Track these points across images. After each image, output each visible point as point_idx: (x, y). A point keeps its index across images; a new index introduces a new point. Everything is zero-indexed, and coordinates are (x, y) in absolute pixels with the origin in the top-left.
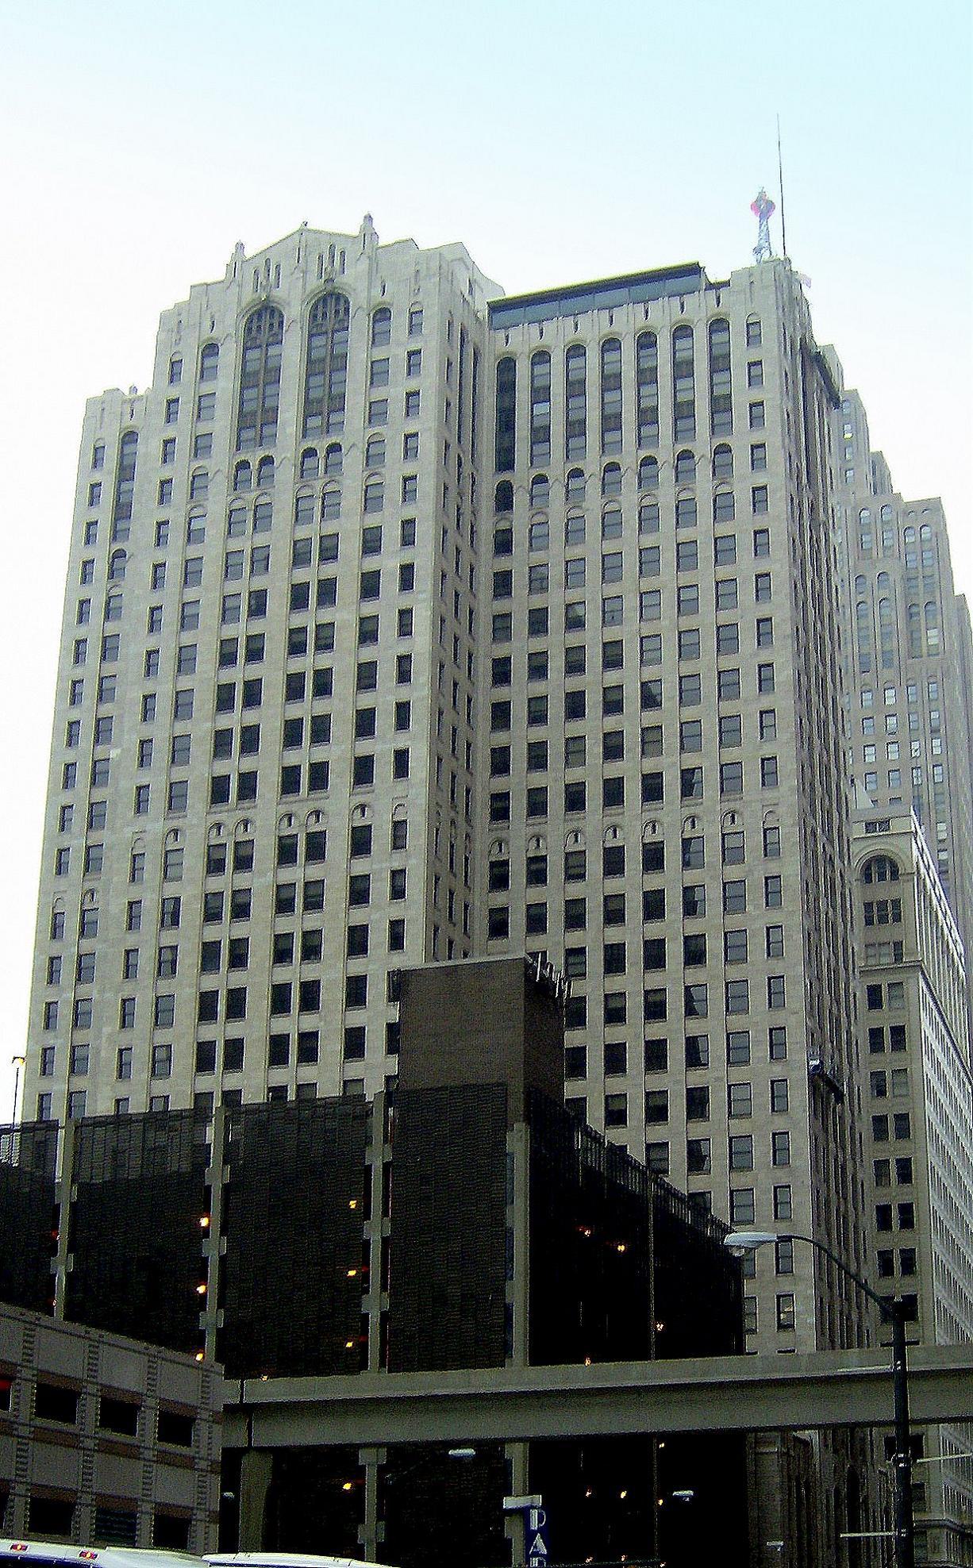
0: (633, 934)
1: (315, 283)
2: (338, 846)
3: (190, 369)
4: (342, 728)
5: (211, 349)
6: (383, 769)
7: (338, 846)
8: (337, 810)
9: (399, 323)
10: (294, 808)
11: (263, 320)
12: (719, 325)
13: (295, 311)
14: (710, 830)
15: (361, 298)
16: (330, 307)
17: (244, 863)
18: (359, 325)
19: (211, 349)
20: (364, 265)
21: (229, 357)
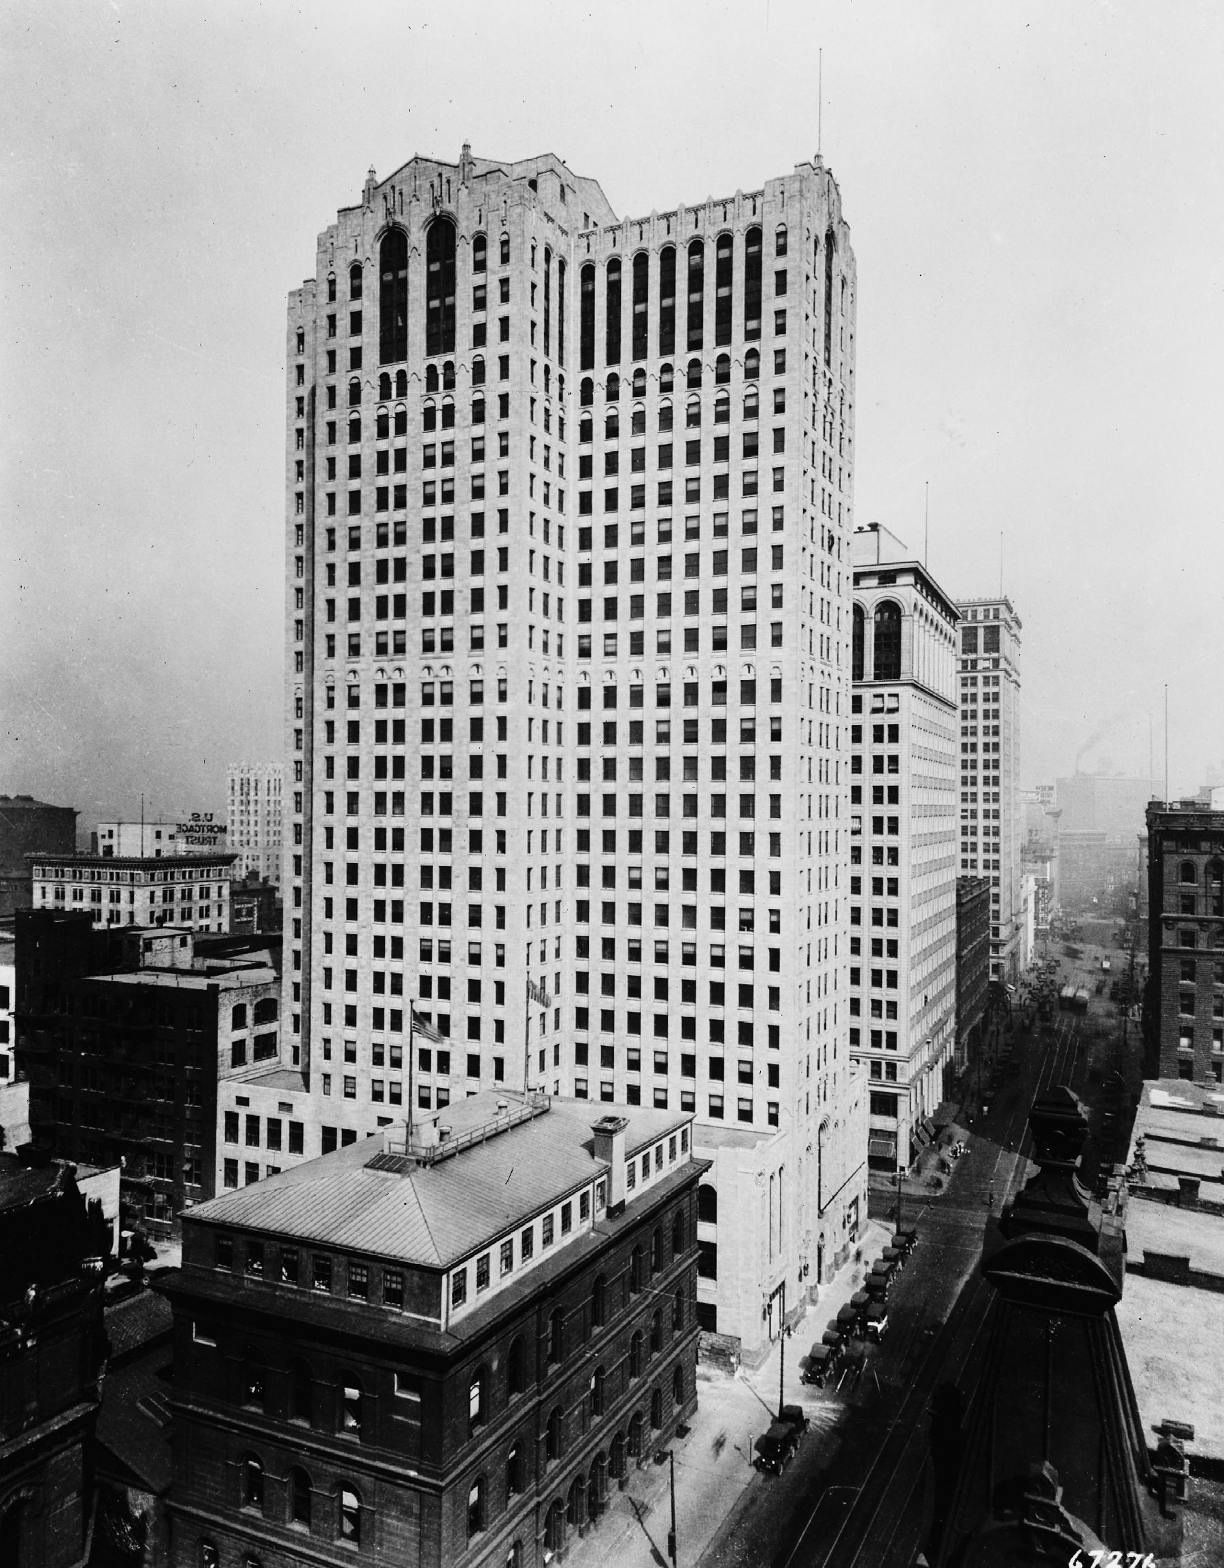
0: (733, 749)
2: (461, 695)
3: (344, 286)
5: (356, 271)
7: (461, 695)
10: (431, 663)
15: (466, 228)
18: (464, 255)
19: (356, 271)
21: (372, 280)
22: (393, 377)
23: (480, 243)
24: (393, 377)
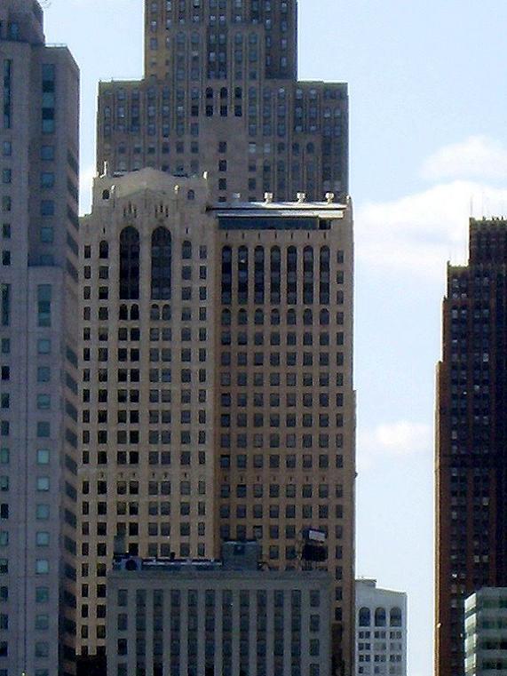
1: (155, 225)
4: (176, 438)
6: (194, 460)
8: (175, 471)
9: (195, 251)
11: (129, 236)
12: (324, 249)
13: (146, 233)
14: (315, 482)
15: (177, 234)
16: (161, 236)
17: (134, 491)
18: (176, 249)
20: (177, 217)
22: (129, 308)
23: (187, 244)
24: (129, 308)
